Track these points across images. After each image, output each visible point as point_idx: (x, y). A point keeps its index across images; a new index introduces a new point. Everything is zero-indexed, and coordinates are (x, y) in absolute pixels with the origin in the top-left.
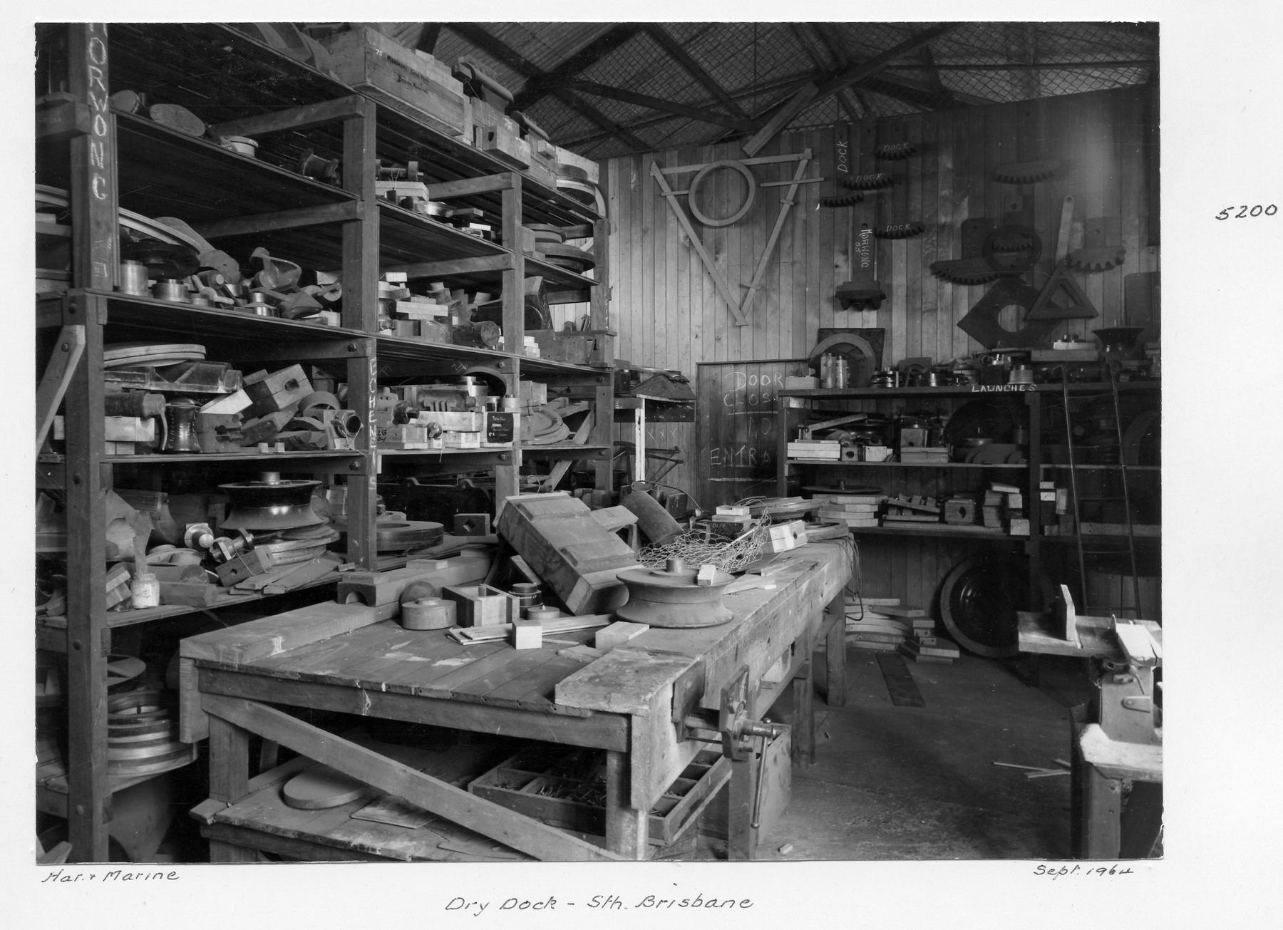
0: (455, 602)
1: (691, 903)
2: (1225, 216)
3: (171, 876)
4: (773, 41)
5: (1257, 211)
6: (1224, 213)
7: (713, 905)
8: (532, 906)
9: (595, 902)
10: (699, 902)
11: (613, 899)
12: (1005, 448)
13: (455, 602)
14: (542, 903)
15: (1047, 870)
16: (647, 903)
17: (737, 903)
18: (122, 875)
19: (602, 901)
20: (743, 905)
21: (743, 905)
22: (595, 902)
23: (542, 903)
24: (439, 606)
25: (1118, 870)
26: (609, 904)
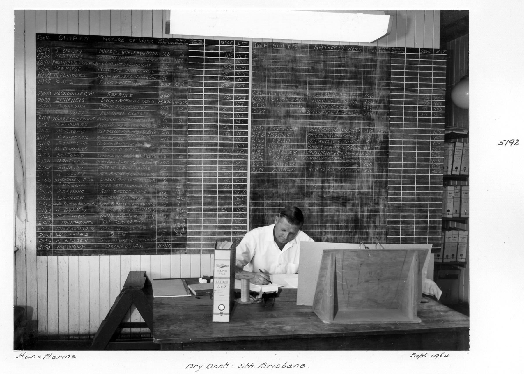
0: (297, 304)
1: (281, 366)
2: (502, 144)
3: (73, 357)
4: (334, 52)
5: (512, 142)
6: (501, 142)
7: (290, 367)
8: (218, 367)
9: (242, 366)
10: (284, 366)
11: (250, 365)
12: (154, 70)
13: (297, 304)
14: (445, 356)
15: (416, 355)
16: (263, 366)
17: (299, 366)
18: (52, 356)
19: (244, 366)
20: (302, 366)
21: (302, 366)
22: (242, 366)
23: (222, 365)
24: (450, 311)
25: (443, 355)
26: (248, 367)
